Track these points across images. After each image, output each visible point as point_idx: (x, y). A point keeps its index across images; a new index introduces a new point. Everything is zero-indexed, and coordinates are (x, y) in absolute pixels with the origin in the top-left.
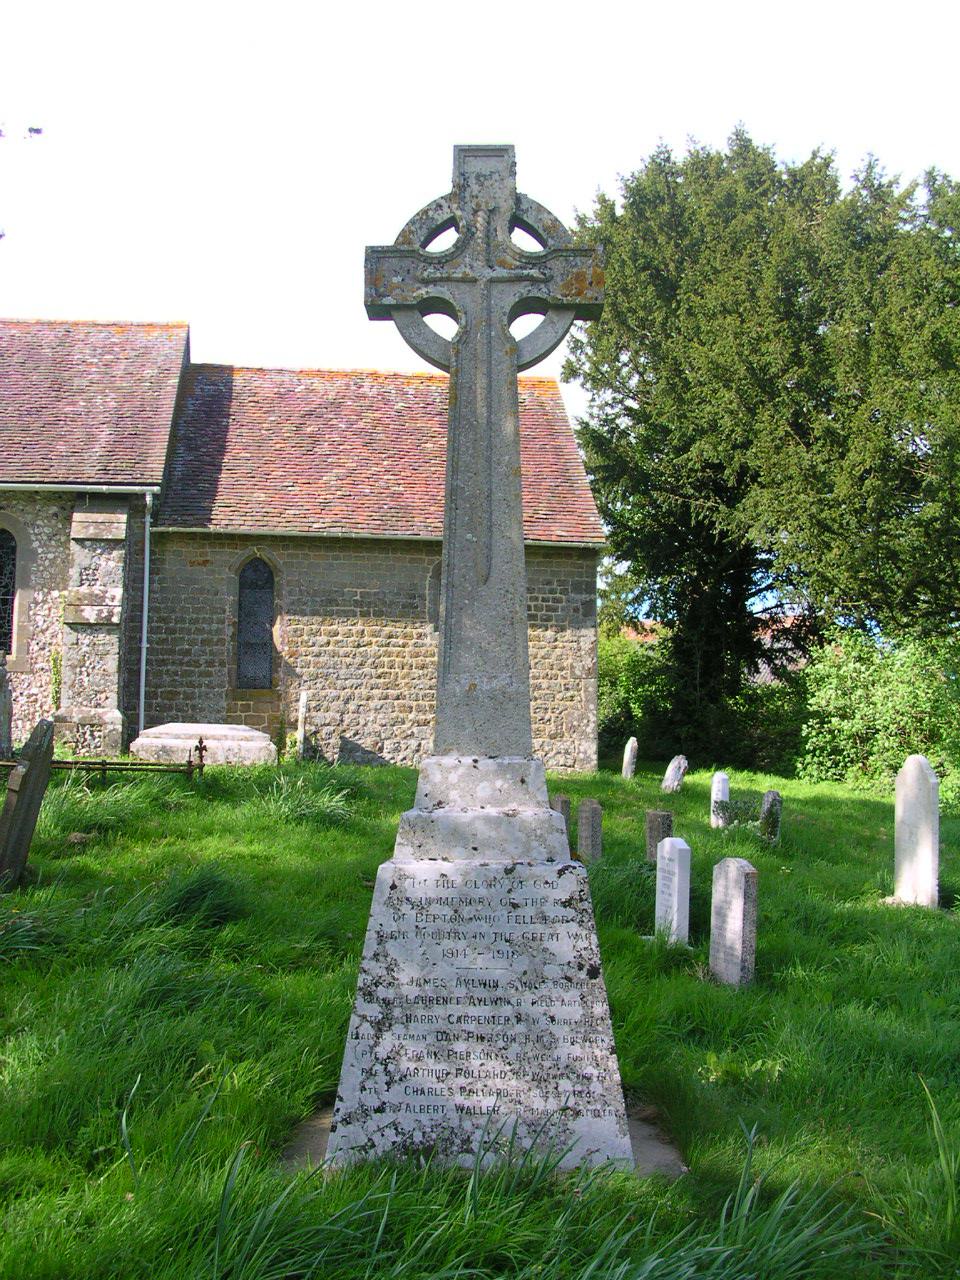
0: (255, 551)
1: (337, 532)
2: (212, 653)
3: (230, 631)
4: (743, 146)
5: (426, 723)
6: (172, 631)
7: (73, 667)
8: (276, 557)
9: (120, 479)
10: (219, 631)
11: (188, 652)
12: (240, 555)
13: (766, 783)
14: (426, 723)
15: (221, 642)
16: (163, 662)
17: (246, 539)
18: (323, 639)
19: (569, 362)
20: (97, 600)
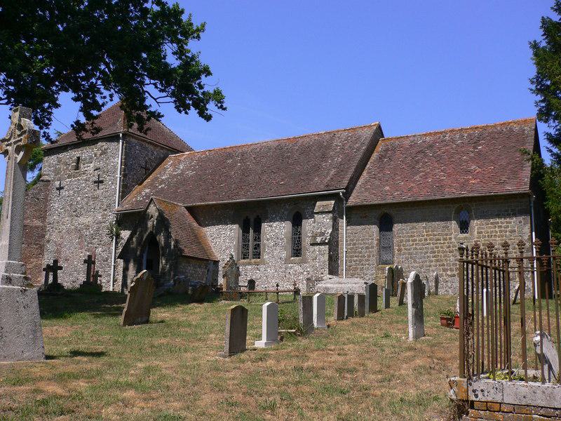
0: (385, 210)
1: (410, 199)
2: (370, 252)
3: (375, 242)
4: (542, 27)
5: (454, 276)
6: (355, 244)
7: (313, 260)
8: (392, 212)
9: (331, 188)
10: (372, 243)
11: (361, 252)
13: (195, 224)
14: (454, 276)
15: (373, 247)
16: (351, 257)
17: (380, 205)
18: (411, 243)
19: (77, 122)
20: (322, 234)
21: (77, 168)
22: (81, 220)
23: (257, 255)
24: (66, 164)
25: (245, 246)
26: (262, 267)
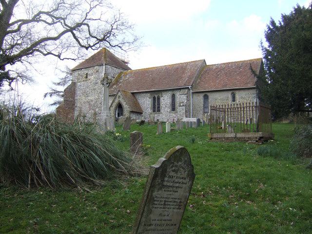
12: (203, 94)
21: (87, 77)
22: (89, 98)
23: (159, 111)
24: (82, 76)
25: (154, 107)
26: (161, 115)
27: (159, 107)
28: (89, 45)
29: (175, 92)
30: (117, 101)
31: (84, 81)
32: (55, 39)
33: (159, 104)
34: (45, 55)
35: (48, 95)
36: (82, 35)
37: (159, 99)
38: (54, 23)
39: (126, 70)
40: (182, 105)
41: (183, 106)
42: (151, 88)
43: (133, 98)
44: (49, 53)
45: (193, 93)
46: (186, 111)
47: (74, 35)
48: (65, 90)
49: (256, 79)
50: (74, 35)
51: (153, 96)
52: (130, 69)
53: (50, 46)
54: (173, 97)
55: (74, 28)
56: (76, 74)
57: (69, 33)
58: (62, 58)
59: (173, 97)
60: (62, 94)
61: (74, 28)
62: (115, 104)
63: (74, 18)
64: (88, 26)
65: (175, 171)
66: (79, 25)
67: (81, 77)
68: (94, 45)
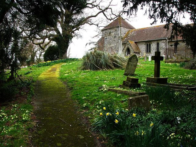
21: (110, 34)
23: (150, 52)
25: (147, 50)
26: (151, 54)
27: (150, 50)
28: (112, 18)
29: (159, 42)
30: (126, 47)
31: (108, 36)
32: (95, 16)
33: (150, 48)
34: (91, 25)
35: (88, 45)
36: (108, 12)
37: (150, 45)
38: (93, 7)
39: (132, 29)
40: (162, 48)
41: (163, 49)
42: (145, 39)
43: (135, 45)
44: (93, 24)
45: (168, 42)
46: (164, 52)
47: (104, 13)
48: (98, 41)
49: (52, 41)
50: (104, 13)
51: (147, 44)
52: (134, 28)
53: (93, 20)
54: (158, 44)
55: (104, 10)
56: (104, 32)
57: (102, 13)
58: (99, 26)
59: (158, 44)
60: (95, 43)
61: (104, 10)
62: (125, 48)
63: (104, 5)
64: (111, 9)
65: (134, 59)
66: (107, 9)
67: (107, 34)
68: (114, 18)
